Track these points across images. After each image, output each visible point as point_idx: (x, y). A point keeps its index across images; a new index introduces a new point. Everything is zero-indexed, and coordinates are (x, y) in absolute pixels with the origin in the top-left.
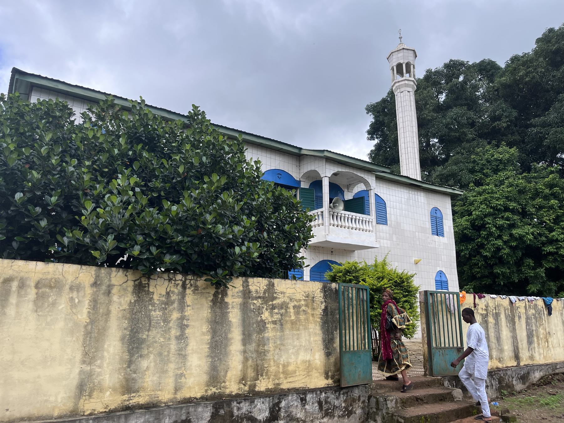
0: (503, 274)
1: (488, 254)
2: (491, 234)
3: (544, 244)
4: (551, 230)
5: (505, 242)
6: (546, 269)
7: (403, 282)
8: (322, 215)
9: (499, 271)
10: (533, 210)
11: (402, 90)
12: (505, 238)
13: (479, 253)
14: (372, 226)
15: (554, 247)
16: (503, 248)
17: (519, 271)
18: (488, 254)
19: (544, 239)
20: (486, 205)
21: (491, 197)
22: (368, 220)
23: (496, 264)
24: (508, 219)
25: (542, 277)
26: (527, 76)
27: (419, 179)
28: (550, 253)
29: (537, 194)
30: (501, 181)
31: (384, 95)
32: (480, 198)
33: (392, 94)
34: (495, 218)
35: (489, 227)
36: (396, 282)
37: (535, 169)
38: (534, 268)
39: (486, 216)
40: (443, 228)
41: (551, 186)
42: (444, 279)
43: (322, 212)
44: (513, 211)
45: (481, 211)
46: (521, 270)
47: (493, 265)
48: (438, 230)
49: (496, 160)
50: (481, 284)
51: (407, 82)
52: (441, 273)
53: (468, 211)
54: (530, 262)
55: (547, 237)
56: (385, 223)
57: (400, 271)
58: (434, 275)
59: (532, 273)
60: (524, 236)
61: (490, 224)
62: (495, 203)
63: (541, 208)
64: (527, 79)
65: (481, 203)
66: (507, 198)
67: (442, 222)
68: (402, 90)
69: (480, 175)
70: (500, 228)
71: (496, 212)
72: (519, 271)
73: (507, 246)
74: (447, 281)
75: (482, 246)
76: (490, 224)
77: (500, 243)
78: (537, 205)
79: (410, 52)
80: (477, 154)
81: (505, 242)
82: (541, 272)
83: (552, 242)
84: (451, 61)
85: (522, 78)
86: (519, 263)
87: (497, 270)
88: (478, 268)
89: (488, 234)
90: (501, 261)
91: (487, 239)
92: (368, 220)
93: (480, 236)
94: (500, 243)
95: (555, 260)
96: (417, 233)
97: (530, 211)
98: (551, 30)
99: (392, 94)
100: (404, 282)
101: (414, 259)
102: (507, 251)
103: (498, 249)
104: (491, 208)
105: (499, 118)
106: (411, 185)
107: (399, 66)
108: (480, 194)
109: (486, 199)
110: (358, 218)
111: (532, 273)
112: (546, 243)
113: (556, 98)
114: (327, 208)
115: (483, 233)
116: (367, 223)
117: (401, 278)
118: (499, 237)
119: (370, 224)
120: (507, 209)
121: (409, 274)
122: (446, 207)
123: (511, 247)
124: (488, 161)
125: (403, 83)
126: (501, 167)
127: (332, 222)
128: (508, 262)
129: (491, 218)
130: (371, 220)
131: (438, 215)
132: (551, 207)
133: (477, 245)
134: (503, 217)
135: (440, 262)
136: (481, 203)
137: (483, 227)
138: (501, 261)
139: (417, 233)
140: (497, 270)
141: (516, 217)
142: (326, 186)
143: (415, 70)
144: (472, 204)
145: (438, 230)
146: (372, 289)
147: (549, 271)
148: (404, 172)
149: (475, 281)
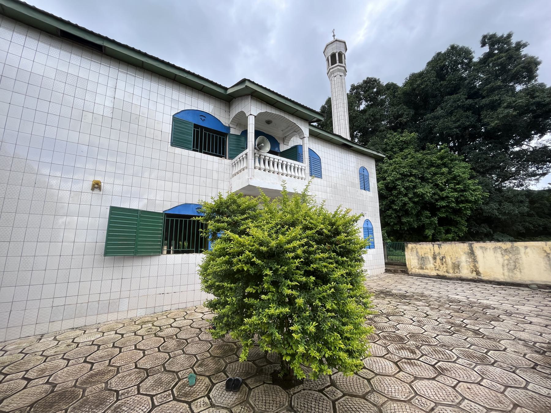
2: (400, 193)
3: (437, 200)
4: (442, 190)
5: (410, 199)
7: (337, 233)
8: (247, 158)
10: (429, 176)
11: (335, 74)
12: (410, 195)
13: (391, 208)
14: (305, 174)
16: (408, 203)
19: (437, 197)
20: (397, 172)
21: (399, 166)
22: (300, 167)
24: (412, 181)
25: (435, 224)
26: (422, 84)
28: (444, 207)
29: (432, 165)
30: (405, 156)
31: (323, 103)
32: (391, 168)
33: (329, 102)
34: (403, 181)
36: (320, 233)
37: (429, 147)
40: (369, 184)
41: (442, 158)
42: (370, 227)
43: (246, 154)
44: (415, 176)
47: (401, 216)
48: (365, 186)
49: (402, 141)
51: (339, 67)
53: (382, 177)
54: (428, 213)
55: (439, 195)
56: (320, 176)
57: (330, 210)
59: (427, 221)
60: (424, 194)
61: (399, 185)
62: (403, 170)
63: (435, 174)
64: (422, 87)
65: (393, 171)
68: (335, 74)
69: (391, 153)
70: (407, 188)
71: (404, 176)
75: (393, 202)
76: (399, 185)
77: (406, 199)
79: (342, 43)
80: (388, 138)
81: (410, 199)
82: (435, 220)
83: (442, 199)
85: (419, 86)
87: (404, 220)
90: (407, 213)
91: (397, 197)
92: (300, 167)
93: (392, 195)
94: (406, 199)
95: (447, 211)
96: (348, 187)
98: (439, 54)
99: (329, 102)
102: (411, 205)
103: (405, 204)
104: (400, 174)
106: (345, 146)
107: (333, 56)
108: (391, 164)
109: (395, 168)
110: (289, 164)
111: (427, 221)
113: (442, 100)
114: (251, 149)
116: (300, 171)
117: (332, 224)
118: (406, 195)
119: (303, 171)
120: (411, 175)
121: (350, 215)
123: (414, 202)
124: (396, 142)
125: (336, 68)
127: (257, 164)
128: (412, 213)
130: (303, 168)
131: (365, 173)
132: (443, 174)
133: (390, 201)
134: (408, 180)
136: (393, 171)
137: (395, 188)
138: (407, 213)
139: (348, 187)
140: (404, 220)
141: (417, 181)
142: (251, 125)
143: (346, 60)
144: (386, 172)
145: (365, 186)
146: (259, 254)
147: (440, 219)
148: (336, 131)
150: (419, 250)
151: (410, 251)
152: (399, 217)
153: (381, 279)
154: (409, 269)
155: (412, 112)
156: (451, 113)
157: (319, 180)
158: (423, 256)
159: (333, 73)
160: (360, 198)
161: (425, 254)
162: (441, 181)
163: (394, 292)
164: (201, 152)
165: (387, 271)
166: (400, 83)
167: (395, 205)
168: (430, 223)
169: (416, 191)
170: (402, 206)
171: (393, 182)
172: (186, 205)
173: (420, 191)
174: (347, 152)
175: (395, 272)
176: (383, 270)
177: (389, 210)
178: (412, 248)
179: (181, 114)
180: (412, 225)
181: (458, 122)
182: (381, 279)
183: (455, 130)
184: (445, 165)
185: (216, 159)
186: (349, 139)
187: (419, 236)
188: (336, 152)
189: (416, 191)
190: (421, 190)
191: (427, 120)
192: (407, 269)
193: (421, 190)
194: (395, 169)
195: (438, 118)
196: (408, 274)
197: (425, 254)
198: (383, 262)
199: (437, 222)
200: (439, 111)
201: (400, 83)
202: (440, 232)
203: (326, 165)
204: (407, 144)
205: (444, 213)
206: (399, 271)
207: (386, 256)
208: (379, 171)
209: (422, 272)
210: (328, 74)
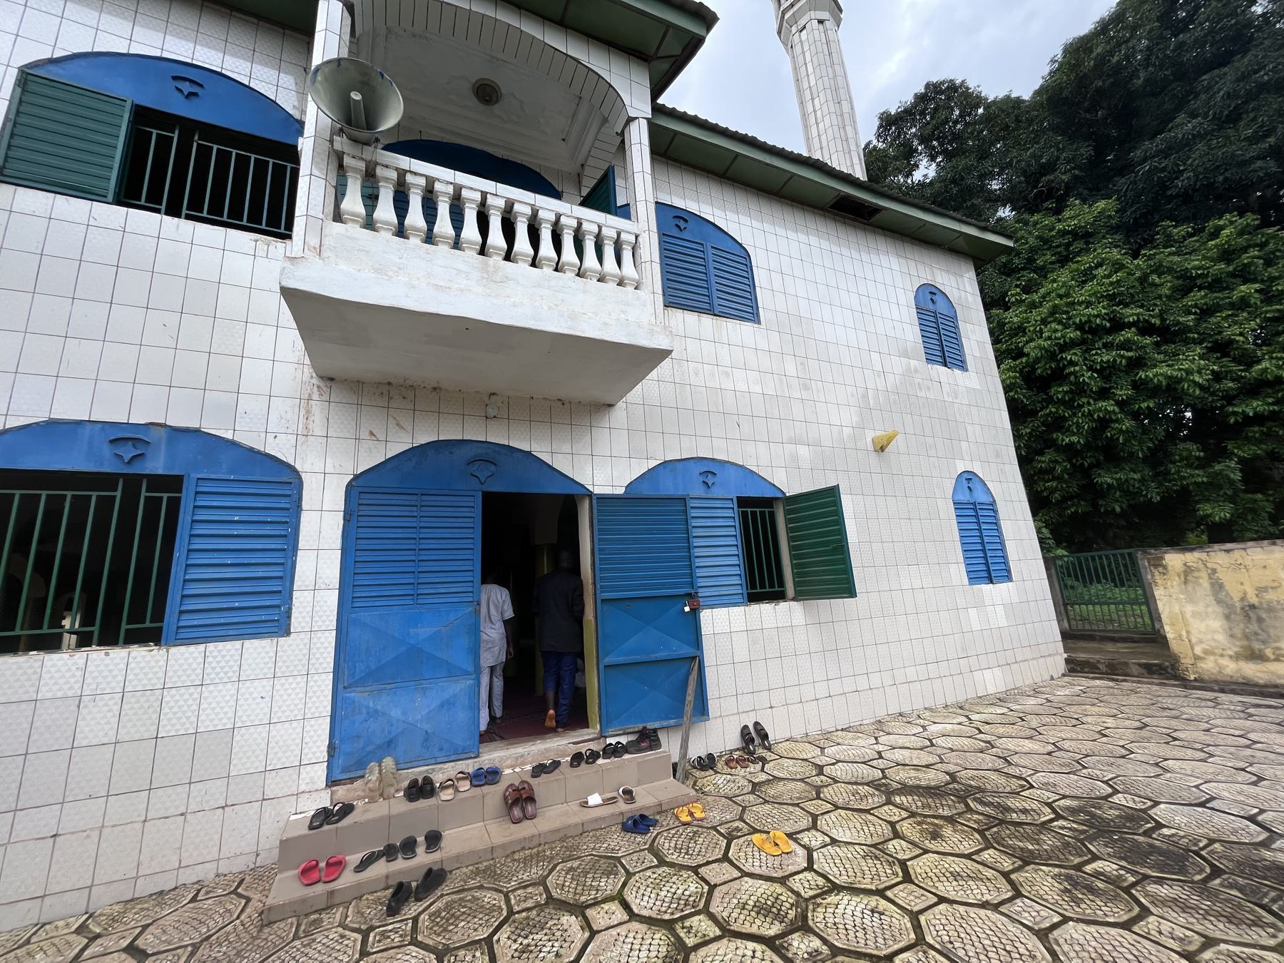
0: (1122, 486)
1: (1075, 439)
2: (1080, 389)
3: (1229, 399)
5: (1121, 404)
6: (1241, 461)
9: (1109, 480)
10: (1189, 320)
11: (801, 23)
12: (1123, 393)
13: (1051, 444)
15: (1270, 400)
17: (1161, 476)
18: (1075, 439)
20: (1060, 322)
23: (1098, 465)
25: (1232, 482)
27: (860, 173)
28: (1259, 419)
35: (1074, 373)
38: (1203, 464)
39: (1065, 347)
41: (1227, 255)
42: (981, 497)
45: (1049, 338)
46: (1167, 473)
47: (1091, 466)
49: (1063, 233)
50: (1059, 515)
52: (968, 478)
58: (949, 485)
59: (1200, 476)
60: (1180, 380)
63: (1206, 312)
65: (1044, 322)
66: (1111, 298)
67: (956, 327)
68: (801, 23)
70: (1106, 372)
71: (1091, 333)
72: (1161, 476)
73: (1126, 414)
74: (993, 503)
75: (1058, 424)
77: (1109, 406)
78: (1196, 306)
82: (1231, 469)
83: (1255, 389)
84: (927, 86)
86: (1157, 459)
87: (1106, 478)
88: (1054, 479)
89: (1071, 392)
90: (1111, 454)
93: (1050, 401)
94: (1109, 406)
97: (1179, 323)
100: (795, 458)
101: (870, 435)
102: (1128, 424)
103: (1105, 423)
105: (1050, 168)
108: (1033, 306)
109: (1055, 310)
111: (1200, 476)
112: (1234, 397)
115: (1060, 391)
118: (1104, 394)
122: (962, 287)
123: (1136, 416)
124: (1045, 241)
126: (1079, 245)
128: (1132, 454)
129: (1078, 351)
131: (941, 307)
132: (1244, 304)
135: (964, 444)
137: (1058, 376)
138: (1111, 454)
140: (1106, 478)
144: (1020, 330)
145: (987, 564)
147: (1248, 466)
149: (1045, 511)
150: (1223, 576)
151: (1176, 581)
152: (1086, 472)
153: (1058, 711)
154: (1186, 661)
155: (1085, 151)
156: (1234, 118)
157: (747, 327)
158: (1253, 600)
159: (795, 19)
160: (931, 395)
161: (1261, 590)
162: (1242, 330)
163: (1178, 820)
164: (174, 211)
165: (1075, 667)
166: (1026, 96)
167: (1068, 431)
168: (1210, 484)
169: (1142, 374)
170: (1092, 430)
171: (1051, 355)
172: (54, 429)
173: (1159, 372)
174: (861, 235)
175: (1114, 671)
176: (1058, 662)
177: (1041, 453)
178: (1188, 571)
179: (68, 65)
180: (1139, 493)
181: (1266, 136)
182: (1058, 711)
183: (1259, 163)
184: (1245, 275)
185: (241, 240)
186: (860, 173)
187: (1176, 523)
188: (814, 240)
189: (1142, 374)
190: (1163, 369)
191: (1145, 160)
192: (1175, 660)
193: (1163, 369)
194: (1052, 314)
195: (1187, 144)
196: (1185, 683)
197: (1261, 590)
198: (1053, 630)
199: (1237, 476)
200: (1185, 126)
201: (1026, 96)
202: (1254, 511)
203: (776, 278)
204: (1085, 236)
205: (1258, 442)
206: (1135, 670)
207: (1064, 604)
208: (992, 302)
209: (1252, 671)
210: (779, 33)
